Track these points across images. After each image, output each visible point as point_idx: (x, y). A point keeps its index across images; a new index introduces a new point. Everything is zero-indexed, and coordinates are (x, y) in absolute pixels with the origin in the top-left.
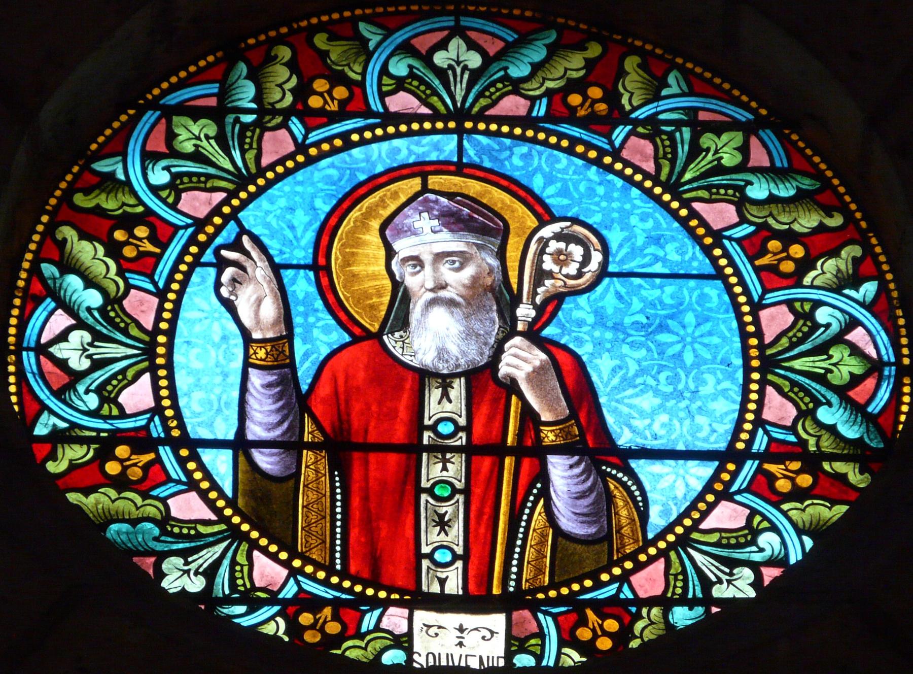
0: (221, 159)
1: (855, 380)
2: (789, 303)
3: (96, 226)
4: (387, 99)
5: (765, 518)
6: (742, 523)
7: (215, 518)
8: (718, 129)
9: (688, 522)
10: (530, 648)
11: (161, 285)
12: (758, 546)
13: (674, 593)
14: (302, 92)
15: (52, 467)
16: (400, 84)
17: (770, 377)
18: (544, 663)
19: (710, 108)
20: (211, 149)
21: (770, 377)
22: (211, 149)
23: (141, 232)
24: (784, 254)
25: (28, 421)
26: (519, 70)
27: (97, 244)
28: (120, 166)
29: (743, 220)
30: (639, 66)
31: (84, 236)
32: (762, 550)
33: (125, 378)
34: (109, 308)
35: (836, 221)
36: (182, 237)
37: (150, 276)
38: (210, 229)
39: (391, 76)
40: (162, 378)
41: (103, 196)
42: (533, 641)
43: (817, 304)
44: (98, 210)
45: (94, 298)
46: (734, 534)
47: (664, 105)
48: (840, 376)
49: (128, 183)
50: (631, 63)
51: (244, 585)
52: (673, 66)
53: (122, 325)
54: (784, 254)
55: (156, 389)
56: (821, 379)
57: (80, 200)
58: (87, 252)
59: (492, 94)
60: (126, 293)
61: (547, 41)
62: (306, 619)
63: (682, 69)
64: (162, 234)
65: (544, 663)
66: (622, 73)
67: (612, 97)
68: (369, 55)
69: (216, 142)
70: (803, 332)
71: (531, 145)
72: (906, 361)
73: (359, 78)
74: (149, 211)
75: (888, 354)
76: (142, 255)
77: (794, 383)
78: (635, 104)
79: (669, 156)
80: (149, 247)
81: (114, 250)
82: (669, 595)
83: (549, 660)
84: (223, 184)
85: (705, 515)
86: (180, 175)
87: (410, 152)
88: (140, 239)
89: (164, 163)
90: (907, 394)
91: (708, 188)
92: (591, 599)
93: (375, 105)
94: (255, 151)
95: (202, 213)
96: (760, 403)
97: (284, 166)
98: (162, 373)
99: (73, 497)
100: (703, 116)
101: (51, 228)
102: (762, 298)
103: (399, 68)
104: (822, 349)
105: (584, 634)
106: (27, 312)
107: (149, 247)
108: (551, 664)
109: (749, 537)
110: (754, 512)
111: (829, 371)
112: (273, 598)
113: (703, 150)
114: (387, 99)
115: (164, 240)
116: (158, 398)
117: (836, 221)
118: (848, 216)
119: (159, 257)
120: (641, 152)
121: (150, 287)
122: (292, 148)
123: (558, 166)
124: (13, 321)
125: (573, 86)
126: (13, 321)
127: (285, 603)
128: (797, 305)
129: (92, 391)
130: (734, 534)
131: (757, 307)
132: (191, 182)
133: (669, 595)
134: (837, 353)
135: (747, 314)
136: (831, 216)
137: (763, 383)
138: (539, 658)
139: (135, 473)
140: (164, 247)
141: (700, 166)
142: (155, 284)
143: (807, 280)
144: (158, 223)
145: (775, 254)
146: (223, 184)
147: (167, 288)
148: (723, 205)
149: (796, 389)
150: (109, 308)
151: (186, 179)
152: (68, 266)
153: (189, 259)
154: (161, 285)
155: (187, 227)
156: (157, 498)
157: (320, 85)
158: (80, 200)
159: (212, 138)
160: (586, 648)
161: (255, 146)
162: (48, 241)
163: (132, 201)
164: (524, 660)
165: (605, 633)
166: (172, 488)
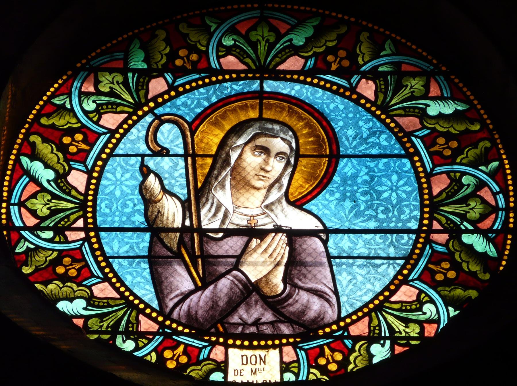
0: (126, 96)
1: (34, 196)
2: (448, 173)
3: (53, 135)
4: (295, 359)
5: (427, 295)
6: (104, 116)
7: (119, 297)
8: (413, 75)
9: (135, 118)
10: (292, 369)
11: (89, 167)
12: (96, 103)
13: (144, 79)
14: (173, 56)
15: (26, 270)
16: (229, 51)
17: (82, 198)
18: (300, 379)
19: (409, 63)
20: (119, 89)
21: (82, 198)
22: (119, 89)
23: (79, 137)
24: (446, 146)
25: (13, 244)
26: (299, 40)
27: (467, 270)
28: (68, 100)
29: (424, 127)
30: (368, 37)
31: (45, 140)
32: (424, 314)
33: (447, 193)
34: (59, 181)
35: (476, 127)
36: (103, 139)
37: (434, 251)
38: (117, 136)
39: (293, 372)
40: (425, 194)
41: (57, 118)
42: (293, 365)
43: (464, 174)
44: (465, 288)
45: (50, 174)
46: (109, 110)
47: (383, 60)
48: (473, 215)
49: (72, 110)
50: (364, 36)
51: (380, 81)
52: (389, 37)
53: (67, 190)
54: (446, 146)
55: (430, 188)
56: (54, 196)
57: (44, 121)
58: (45, 149)
59: (283, 56)
60: (69, 173)
61: (314, 24)
62: (346, 63)
63: (394, 41)
64: (91, 138)
65: (300, 379)
66: (358, 41)
67: (353, 57)
68: (211, 35)
69: (394, 329)
70: (455, 190)
71: (302, 85)
72: (512, 205)
73: (312, 370)
74: (83, 126)
75: (14, 210)
76: (80, 151)
77: (69, 194)
78: (366, 60)
79: (383, 90)
80: (83, 146)
81: (63, 148)
82: (147, 79)
83: (302, 377)
84: (126, 109)
85: (125, 121)
86: (102, 105)
87: (232, 89)
88: (78, 142)
89: (93, 98)
90: (511, 223)
91: (109, 306)
92: (327, 339)
93: (214, 64)
94: (145, 91)
95: (404, 288)
96: (89, 183)
97: (358, 316)
98: (426, 197)
99: (39, 286)
100: (404, 68)
101: (27, 135)
102: (432, 170)
103: (228, 42)
104: (464, 201)
105: (322, 361)
106: (13, 184)
107: (83, 146)
108: (304, 378)
109: (418, 306)
110: (421, 292)
111: (467, 212)
112: (365, 75)
113: (404, 86)
114: (295, 359)
115: (426, 272)
116: (428, 182)
117: (476, 127)
118: (484, 125)
119: (89, 152)
120: (368, 89)
121: (83, 169)
122: (166, 88)
123: (317, 96)
124: (5, 189)
125: (329, 51)
126: (5, 189)
127: (358, 73)
128: (452, 175)
129: (466, 185)
130: (109, 110)
131: (429, 176)
132: (107, 108)
133: (147, 79)
134: (46, 212)
135: (423, 179)
136: (473, 124)
137: (86, 195)
138: (297, 375)
139: (441, 141)
140: (92, 145)
141: (111, 320)
142: (86, 167)
143: (55, 254)
144: (88, 133)
145: (441, 145)
146: (126, 109)
147: (424, 245)
148: (99, 296)
149: (449, 222)
150: (59, 181)
151: (105, 107)
152: (34, 156)
153: (412, 262)
154: (89, 167)
155: (413, 280)
156: (85, 286)
157: (182, 53)
158: (44, 121)
159: (121, 84)
160: (323, 369)
161: (145, 87)
162: (26, 143)
163: (74, 121)
164: (289, 377)
165: (335, 361)
166: (94, 281)
